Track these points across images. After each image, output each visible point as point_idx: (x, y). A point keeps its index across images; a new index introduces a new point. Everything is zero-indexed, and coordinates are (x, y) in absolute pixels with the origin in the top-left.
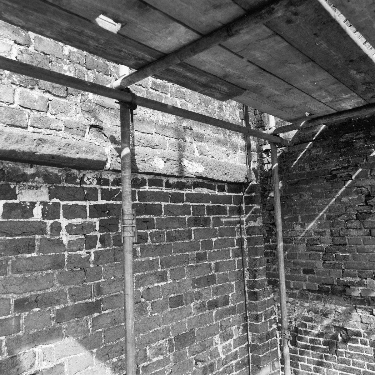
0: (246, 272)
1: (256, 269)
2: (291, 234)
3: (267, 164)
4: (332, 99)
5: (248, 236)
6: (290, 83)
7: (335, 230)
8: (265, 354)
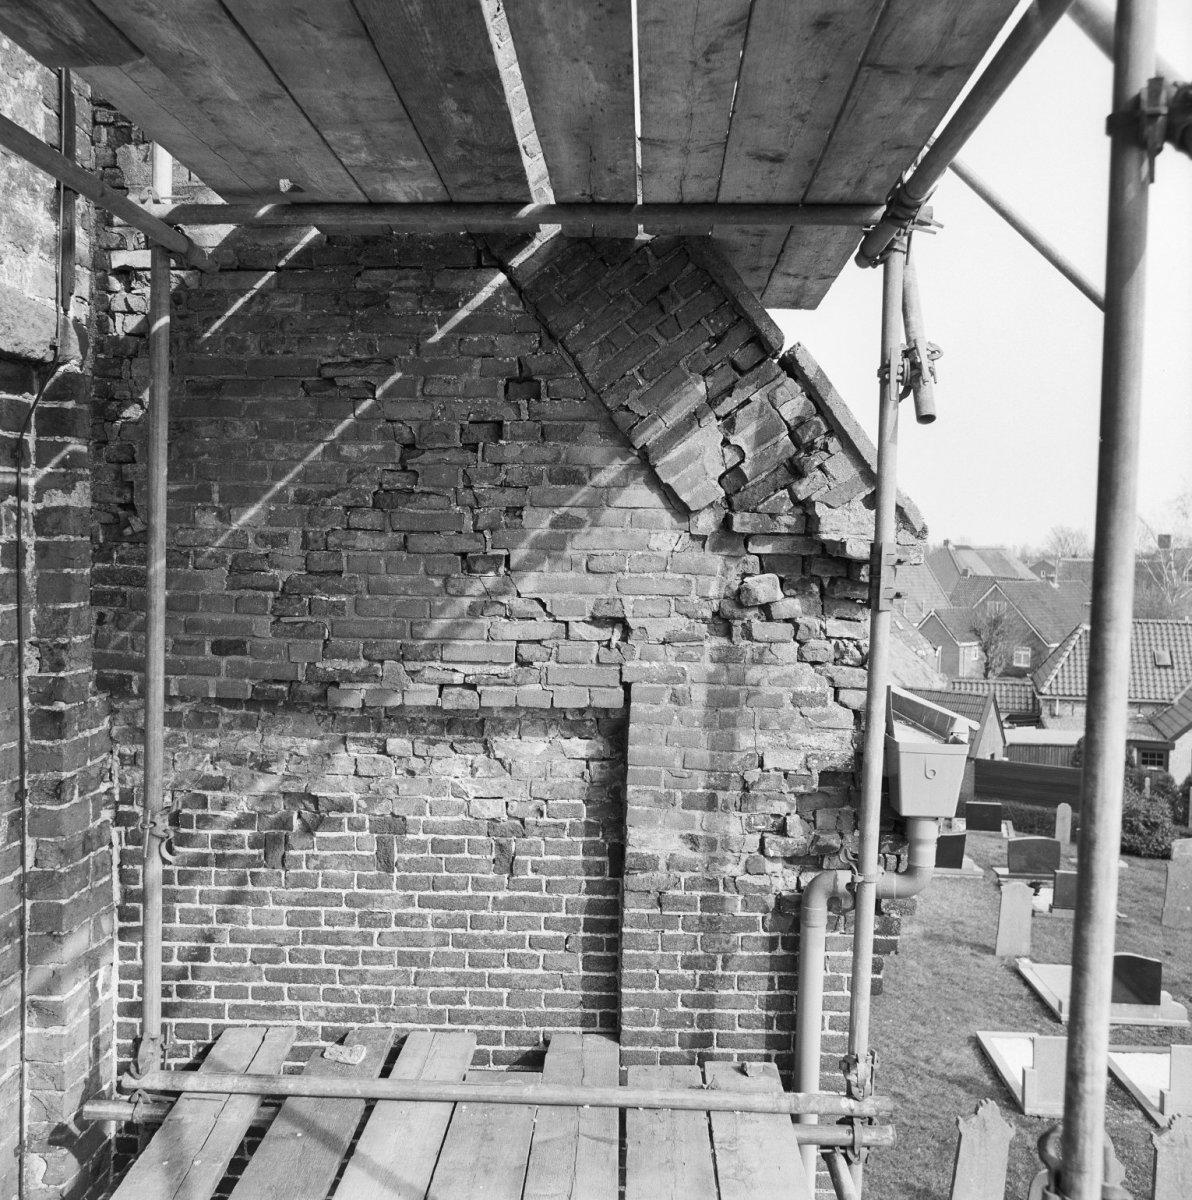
0: (26, 651)
1: (63, 641)
2: (185, 536)
3: (123, 313)
4: (370, 159)
5: (42, 539)
6: (282, 78)
7: (315, 533)
8: (76, 895)
